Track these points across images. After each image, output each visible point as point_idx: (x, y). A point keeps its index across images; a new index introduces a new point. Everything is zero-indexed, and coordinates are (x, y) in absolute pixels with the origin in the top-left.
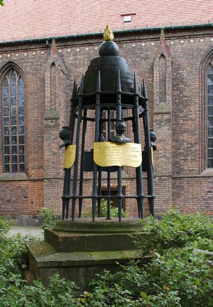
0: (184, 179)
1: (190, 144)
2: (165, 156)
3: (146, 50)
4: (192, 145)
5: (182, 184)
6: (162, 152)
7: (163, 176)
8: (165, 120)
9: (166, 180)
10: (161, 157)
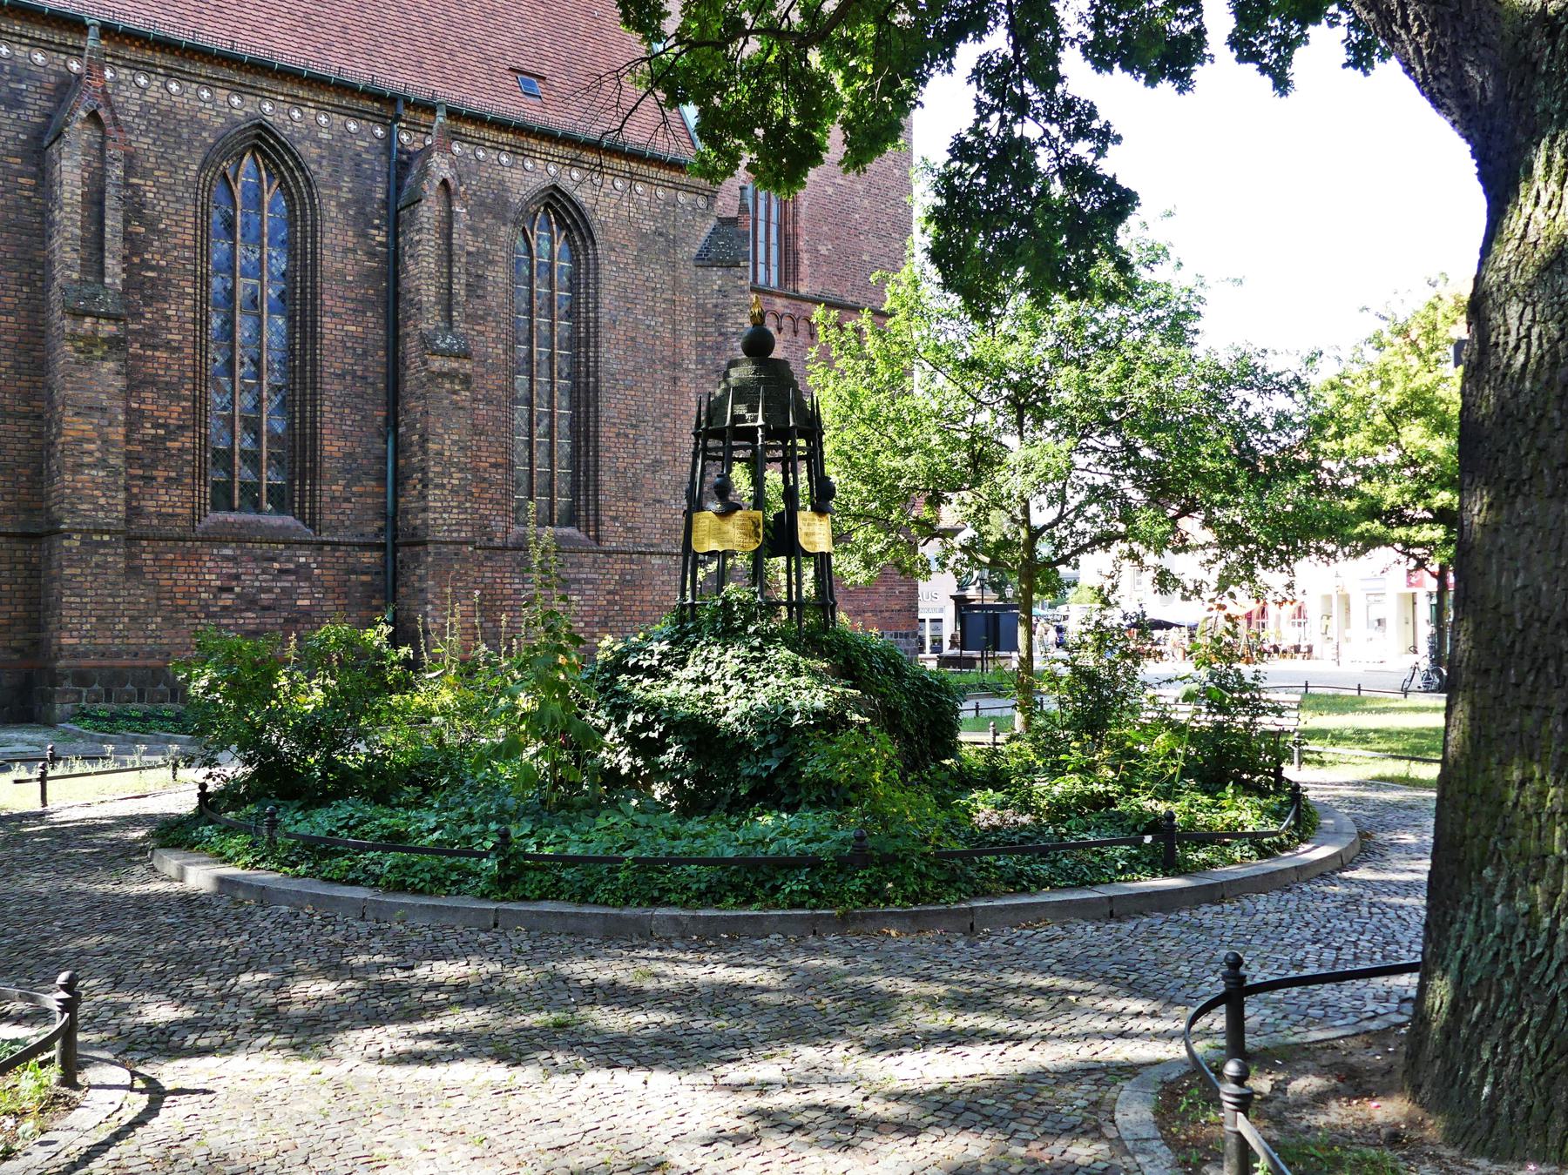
0: (145, 543)
1: (165, 426)
2: (102, 464)
3: (12, 73)
4: (172, 433)
5: (137, 562)
6: (93, 447)
7: (96, 532)
8: (104, 340)
9: (104, 544)
10: (90, 466)
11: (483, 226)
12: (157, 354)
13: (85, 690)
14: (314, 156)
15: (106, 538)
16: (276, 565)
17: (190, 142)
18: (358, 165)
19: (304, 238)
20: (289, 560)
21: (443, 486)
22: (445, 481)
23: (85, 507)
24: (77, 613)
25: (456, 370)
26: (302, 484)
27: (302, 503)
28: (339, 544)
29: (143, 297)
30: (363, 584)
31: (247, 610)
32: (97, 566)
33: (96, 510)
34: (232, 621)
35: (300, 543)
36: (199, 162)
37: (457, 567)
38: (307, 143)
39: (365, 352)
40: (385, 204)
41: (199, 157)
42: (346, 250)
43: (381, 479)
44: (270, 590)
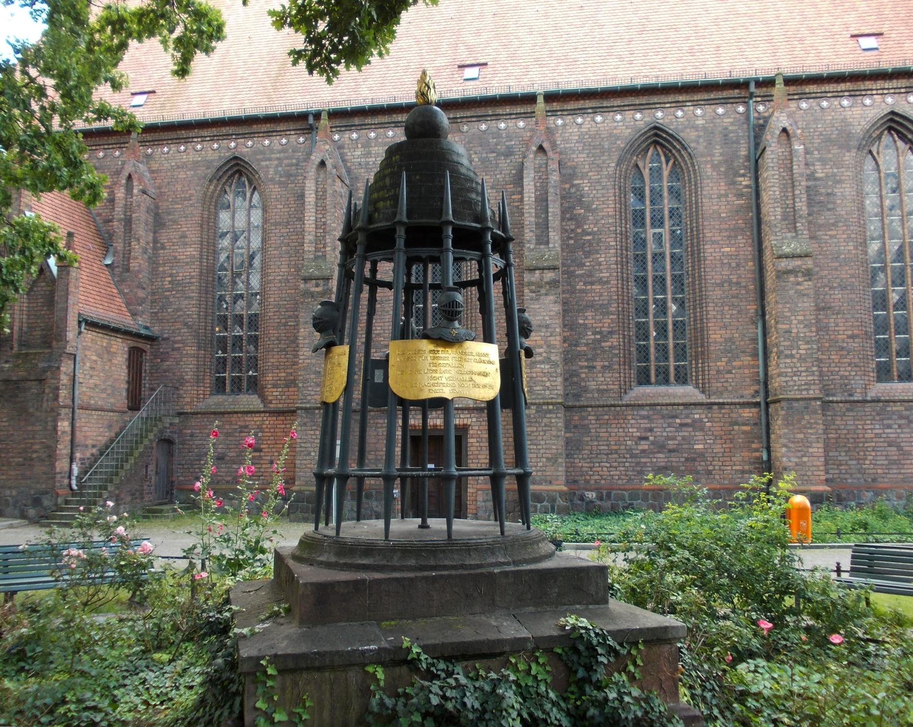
0: (590, 409)
1: (600, 333)
2: (547, 360)
4: (605, 336)
5: (586, 422)
6: (541, 350)
8: (547, 283)
10: (542, 362)
11: (830, 156)
12: (594, 287)
13: (539, 505)
14: (693, 138)
15: (551, 407)
16: (678, 421)
17: (609, 150)
18: (726, 135)
19: (690, 195)
20: (687, 417)
21: (792, 356)
22: (794, 352)
23: (538, 388)
24: (535, 455)
25: (799, 266)
26: (697, 364)
27: (697, 376)
28: (723, 404)
29: (584, 252)
30: (744, 432)
31: (659, 452)
32: (546, 426)
33: (544, 390)
34: (648, 460)
35: (695, 404)
36: (615, 160)
37: (807, 417)
38: (688, 130)
39: (738, 265)
40: (748, 158)
41: (615, 157)
42: (720, 197)
43: (755, 355)
44: (674, 438)
